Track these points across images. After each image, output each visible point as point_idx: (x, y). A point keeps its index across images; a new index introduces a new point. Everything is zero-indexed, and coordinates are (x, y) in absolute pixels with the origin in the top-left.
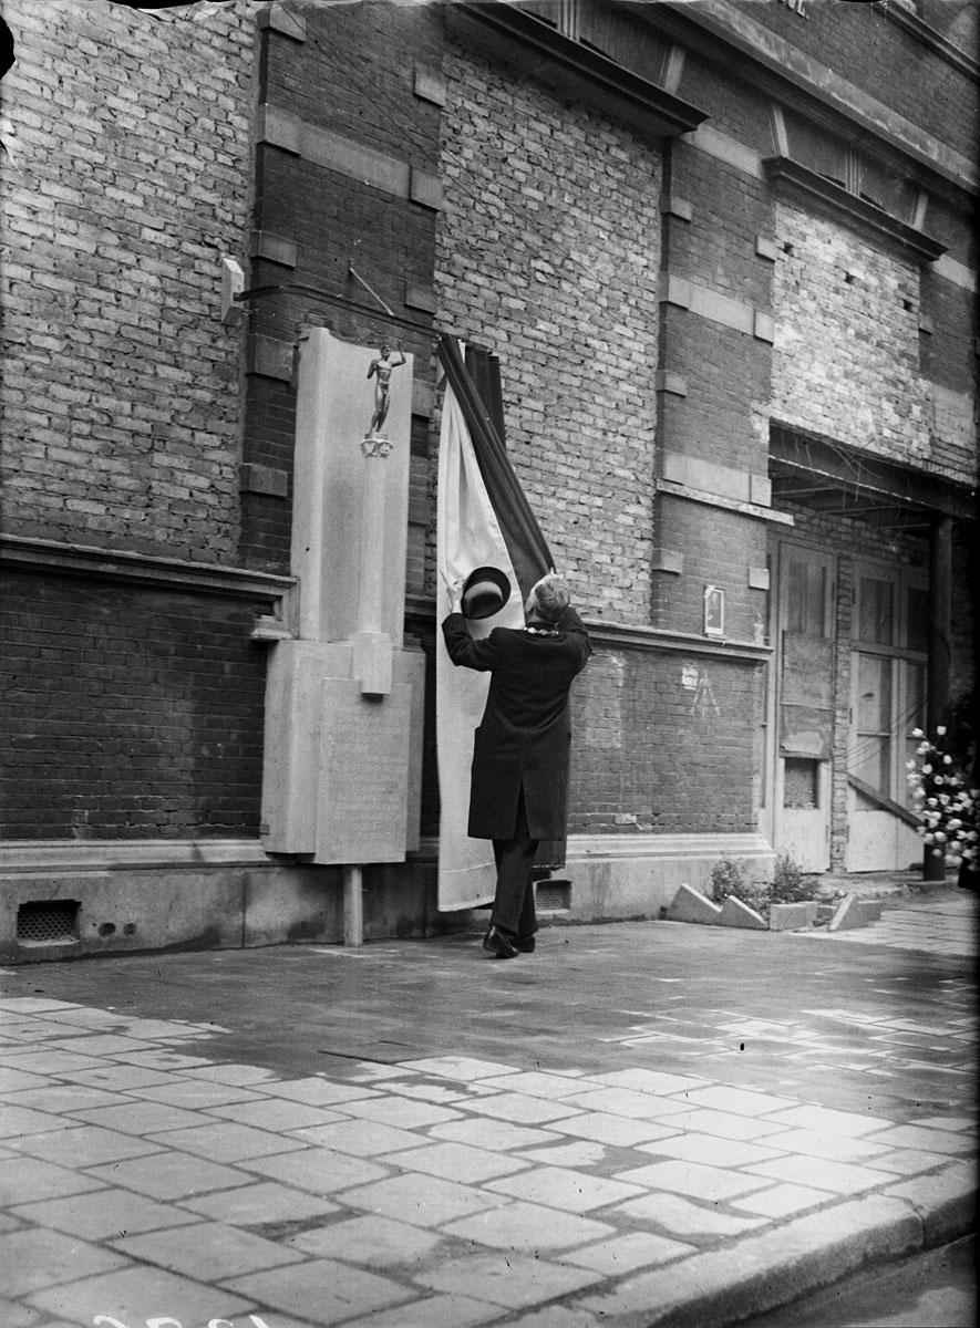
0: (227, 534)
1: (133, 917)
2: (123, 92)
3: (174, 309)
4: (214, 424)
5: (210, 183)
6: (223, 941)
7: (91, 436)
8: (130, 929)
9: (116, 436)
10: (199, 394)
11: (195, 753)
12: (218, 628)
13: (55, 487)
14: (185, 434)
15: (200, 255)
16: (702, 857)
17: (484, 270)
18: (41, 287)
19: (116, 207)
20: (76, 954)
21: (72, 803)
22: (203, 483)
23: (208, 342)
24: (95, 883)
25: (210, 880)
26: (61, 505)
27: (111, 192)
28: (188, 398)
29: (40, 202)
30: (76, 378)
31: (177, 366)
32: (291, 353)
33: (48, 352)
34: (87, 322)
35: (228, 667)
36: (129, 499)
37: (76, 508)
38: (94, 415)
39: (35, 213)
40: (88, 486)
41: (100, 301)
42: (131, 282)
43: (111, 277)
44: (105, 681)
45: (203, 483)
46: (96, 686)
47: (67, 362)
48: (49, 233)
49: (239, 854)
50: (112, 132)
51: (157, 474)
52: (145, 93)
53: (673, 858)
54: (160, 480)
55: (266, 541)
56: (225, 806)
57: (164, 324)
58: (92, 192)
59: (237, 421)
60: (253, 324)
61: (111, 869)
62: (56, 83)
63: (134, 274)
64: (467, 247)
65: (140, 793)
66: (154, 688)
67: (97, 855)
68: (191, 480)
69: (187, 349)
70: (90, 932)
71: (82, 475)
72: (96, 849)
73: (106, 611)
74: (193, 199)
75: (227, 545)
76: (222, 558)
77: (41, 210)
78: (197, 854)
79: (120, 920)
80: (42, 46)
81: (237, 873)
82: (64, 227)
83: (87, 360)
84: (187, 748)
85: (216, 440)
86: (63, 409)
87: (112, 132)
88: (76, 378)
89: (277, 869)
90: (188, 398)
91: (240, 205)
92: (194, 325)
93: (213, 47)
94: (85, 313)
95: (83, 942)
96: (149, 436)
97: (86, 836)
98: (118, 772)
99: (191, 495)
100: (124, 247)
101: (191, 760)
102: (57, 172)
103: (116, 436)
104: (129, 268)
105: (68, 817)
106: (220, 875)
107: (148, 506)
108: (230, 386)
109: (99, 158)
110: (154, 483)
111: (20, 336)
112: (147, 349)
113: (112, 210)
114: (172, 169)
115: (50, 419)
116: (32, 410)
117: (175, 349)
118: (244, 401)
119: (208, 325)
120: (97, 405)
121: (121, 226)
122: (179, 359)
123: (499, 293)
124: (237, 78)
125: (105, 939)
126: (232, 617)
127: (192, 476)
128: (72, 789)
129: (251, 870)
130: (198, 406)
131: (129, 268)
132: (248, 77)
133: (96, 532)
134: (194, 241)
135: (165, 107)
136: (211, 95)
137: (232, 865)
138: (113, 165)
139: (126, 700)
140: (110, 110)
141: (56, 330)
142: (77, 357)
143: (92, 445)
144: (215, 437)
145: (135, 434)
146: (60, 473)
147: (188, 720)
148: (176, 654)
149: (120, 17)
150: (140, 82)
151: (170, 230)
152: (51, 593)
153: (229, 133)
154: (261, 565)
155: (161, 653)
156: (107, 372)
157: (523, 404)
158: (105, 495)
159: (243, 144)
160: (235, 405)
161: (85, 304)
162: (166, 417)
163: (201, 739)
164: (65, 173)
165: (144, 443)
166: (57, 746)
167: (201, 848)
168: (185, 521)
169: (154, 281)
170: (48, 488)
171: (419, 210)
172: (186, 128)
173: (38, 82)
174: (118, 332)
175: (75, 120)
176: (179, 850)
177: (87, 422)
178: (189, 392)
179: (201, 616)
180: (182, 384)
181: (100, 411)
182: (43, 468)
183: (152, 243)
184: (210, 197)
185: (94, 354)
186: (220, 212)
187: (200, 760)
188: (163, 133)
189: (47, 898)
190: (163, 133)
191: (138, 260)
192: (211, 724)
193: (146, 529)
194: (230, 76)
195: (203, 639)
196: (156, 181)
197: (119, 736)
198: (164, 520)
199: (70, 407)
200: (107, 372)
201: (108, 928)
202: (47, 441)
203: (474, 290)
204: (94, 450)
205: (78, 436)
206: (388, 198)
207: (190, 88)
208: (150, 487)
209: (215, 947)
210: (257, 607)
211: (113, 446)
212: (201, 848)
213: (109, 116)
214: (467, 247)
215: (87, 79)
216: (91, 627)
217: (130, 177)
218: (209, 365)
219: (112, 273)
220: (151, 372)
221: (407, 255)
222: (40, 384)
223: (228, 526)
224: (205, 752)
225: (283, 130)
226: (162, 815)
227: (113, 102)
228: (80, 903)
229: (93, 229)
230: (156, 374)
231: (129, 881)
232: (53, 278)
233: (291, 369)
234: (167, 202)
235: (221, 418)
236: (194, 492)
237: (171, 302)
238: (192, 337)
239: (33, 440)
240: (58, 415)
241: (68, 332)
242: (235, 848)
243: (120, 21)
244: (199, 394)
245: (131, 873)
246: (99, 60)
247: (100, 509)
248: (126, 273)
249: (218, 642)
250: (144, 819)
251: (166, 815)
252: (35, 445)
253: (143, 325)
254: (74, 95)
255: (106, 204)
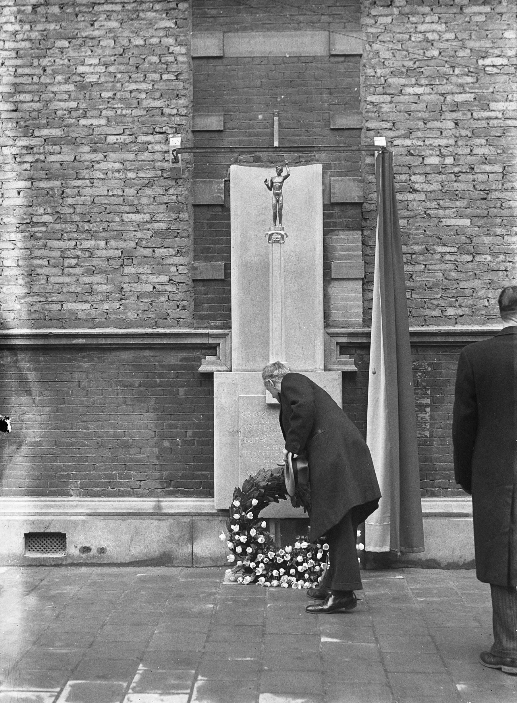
0: (184, 308)
1: (103, 545)
2: (88, 61)
3: (134, 179)
4: (170, 241)
5: (158, 94)
6: (175, 561)
7: (77, 265)
8: (102, 550)
9: (95, 262)
10: (156, 225)
11: (158, 445)
12: (172, 367)
13: (54, 298)
14: (147, 252)
15: (153, 141)
16: (8, 518)
17: (423, 81)
18: (38, 189)
19: (86, 129)
20: (64, 563)
21: (68, 476)
22: (164, 279)
23: (162, 192)
24: (75, 524)
25: (162, 523)
26: (60, 307)
27: (83, 122)
28: (148, 230)
29: (34, 142)
30: (65, 235)
31: (138, 212)
32: (222, 185)
33: (45, 224)
34: (70, 201)
35: (182, 391)
36: (107, 297)
37: (69, 308)
38: (79, 253)
39: (32, 148)
40: (77, 294)
41: (78, 187)
42: (100, 170)
43: (85, 171)
44: (88, 406)
45: (164, 279)
46: (81, 410)
47: (58, 227)
48: (42, 157)
49: (194, 507)
50: (82, 87)
51: (127, 279)
52: (104, 56)
53: (58, 518)
54: (129, 283)
55: (210, 309)
56: (184, 477)
57: (126, 190)
58: (69, 126)
59: (188, 237)
60: (197, 174)
61: (88, 515)
62: (42, 72)
63: (103, 166)
64: (404, 70)
65: (117, 470)
66: (124, 407)
67: (82, 506)
68: (153, 279)
69: (144, 201)
70: (73, 550)
71: (73, 288)
72: (12, 503)
73: (86, 366)
74: (144, 109)
75: (184, 314)
76: (181, 323)
77: (35, 146)
78: (159, 507)
79: (94, 545)
80: (31, 54)
81: (187, 519)
82: (52, 151)
83: (72, 222)
84: (152, 442)
85: (172, 251)
86: (58, 254)
87: (82, 87)
88: (65, 235)
89: (220, 518)
90: (148, 230)
91: (182, 101)
92: (150, 184)
93: (156, 11)
94: (69, 196)
95: (68, 556)
96: (120, 258)
97: (79, 495)
98: (100, 458)
99: (154, 288)
100: (95, 151)
101: (156, 450)
102: (45, 122)
103: (95, 262)
104: (98, 162)
105: (67, 484)
106: (171, 520)
107: (121, 299)
108: (181, 216)
109: (73, 104)
110: (125, 286)
111: (26, 219)
112: (115, 207)
113: (85, 132)
114: (128, 95)
115: (48, 261)
116: (36, 258)
117: (136, 202)
118: (192, 223)
119: (162, 182)
120: (80, 247)
121: (91, 140)
122: (139, 208)
123: (442, 95)
124: (176, 23)
125: (84, 555)
126: (184, 359)
127: (155, 277)
128: (67, 468)
129: (197, 518)
130: (156, 233)
131: (98, 162)
132: (185, 19)
133: (85, 320)
134: (146, 134)
135: (121, 60)
136: (154, 41)
137: (184, 515)
138: (83, 106)
139: (103, 416)
140: (79, 75)
141: (49, 210)
142: (65, 222)
143: (78, 271)
144: (171, 249)
145: (109, 259)
146: (58, 290)
147: (151, 425)
148: (140, 386)
149: (83, 19)
150: (99, 51)
151: (127, 132)
152: (47, 359)
153: (170, 59)
154: (206, 325)
155: (131, 386)
156: (87, 226)
157: (476, 170)
158: (90, 298)
159: (183, 63)
160: (186, 227)
161: (68, 191)
162: (133, 244)
163: (163, 436)
164: (51, 121)
165: (115, 264)
166: (55, 444)
167: (162, 504)
168: (151, 304)
169: (117, 166)
170: (50, 300)
171: (342, 59)
172: (137, 67)
173: (29, 75)
174: (93, 202)
175: (55, 89)
176: (147, 504)
177: (74, 258)
178: (149, 226)
179: (159, 362)
180: (143, 222)
181: (82, 250)
182: (46, 289)
183: (115, 143)
184: (158, 104)
185: (77, 218)
186: (167, 111)
187: (162, 450)
188: (119, 76)
189: (43, 531)
190: (119, 76)
191: (105, 157)
192: (170, 426)
193: (121, 313)
194: (170, 24)
195: (160, 376)
196: (116, 106)
197: (100, 437)
198: (134, 306)
199: (62, 252)
200: (87, 226)
201: (86, 549)
202: (47, 273)
203: (412, 99)
204: (80, 273)
205: (69, 267)
206: (310, 59)
207: (139, 42)
208: (122, 288)
209: (170, 565)
210: (203, 351)
211: (94, 268)
212: (162, 504)
213: (78, 79)
214: (404, 70)
215: (62, 62)
216: (75, 375)
217: (95, 109)
218: (164, 206)
219: (86, 169)
220: (119, 220)
221: (331, 94)
222: (41, 243)
223: (184, 303)
224: (166, 444)
225: (208, 45)
226: (133, 482)
227: (81, 69)
228: (65, 534)
229: (71, 147)
230: (122, 220)
231: (100, 523)
232: (45, 182)
233: (223, 196)
234: (125, 116)
235: (176, 237)
236: (157, 286)
237: (131, 175)
238: (149, 192)
239: (38, 275)
240: (54, 258)
241: (57, 210)
242: (208, 503)
243: (84, 21)
244: (156, 225)
245: (102, 518)
246: (70, 49)
247: (87, 306)
248: (96, 166)
249: (173, 376)
250: (122, 485)
251: (138, 483)
252: (40, 277)
253: (110, 193)
254: (55, 73)
255: (79, 130)
